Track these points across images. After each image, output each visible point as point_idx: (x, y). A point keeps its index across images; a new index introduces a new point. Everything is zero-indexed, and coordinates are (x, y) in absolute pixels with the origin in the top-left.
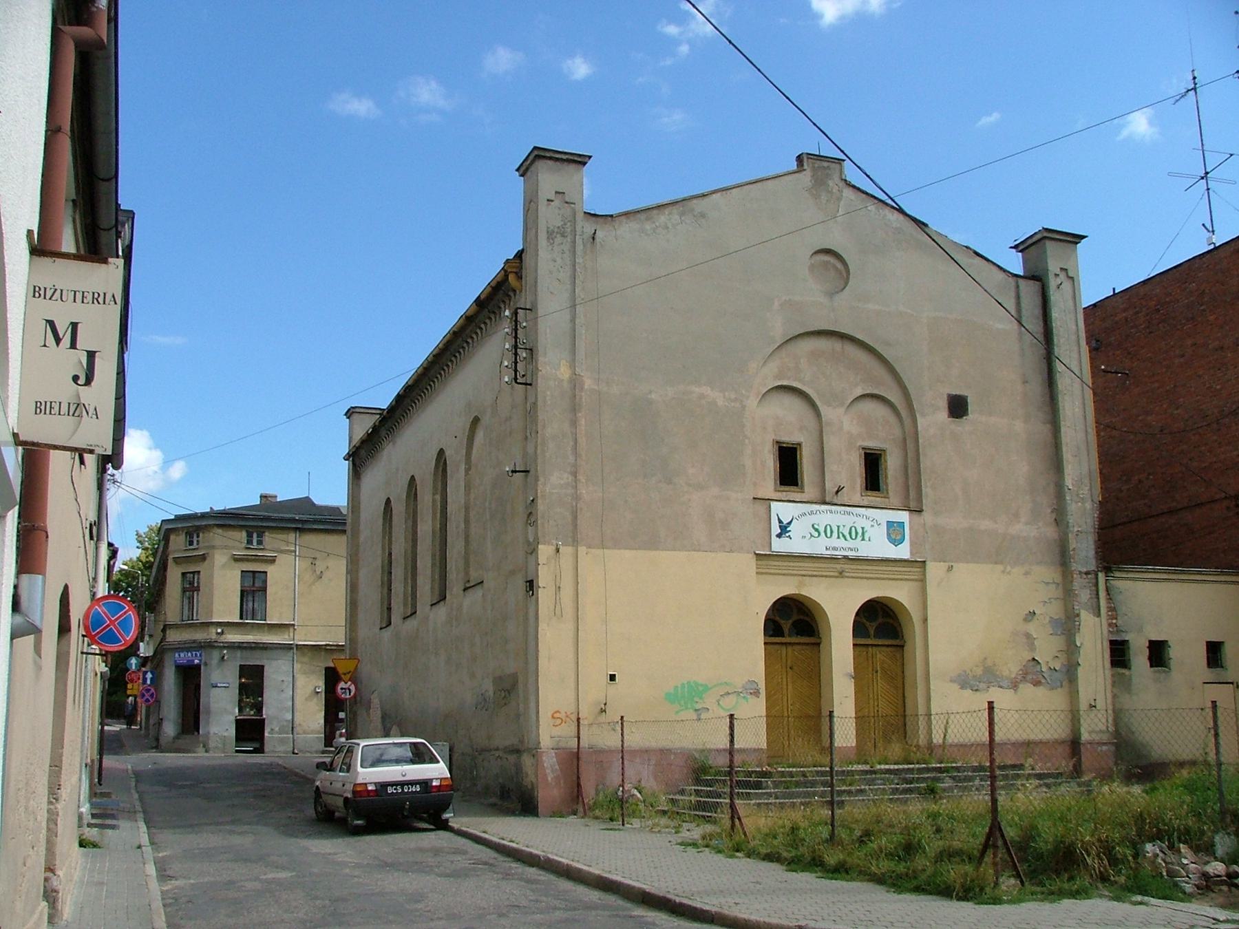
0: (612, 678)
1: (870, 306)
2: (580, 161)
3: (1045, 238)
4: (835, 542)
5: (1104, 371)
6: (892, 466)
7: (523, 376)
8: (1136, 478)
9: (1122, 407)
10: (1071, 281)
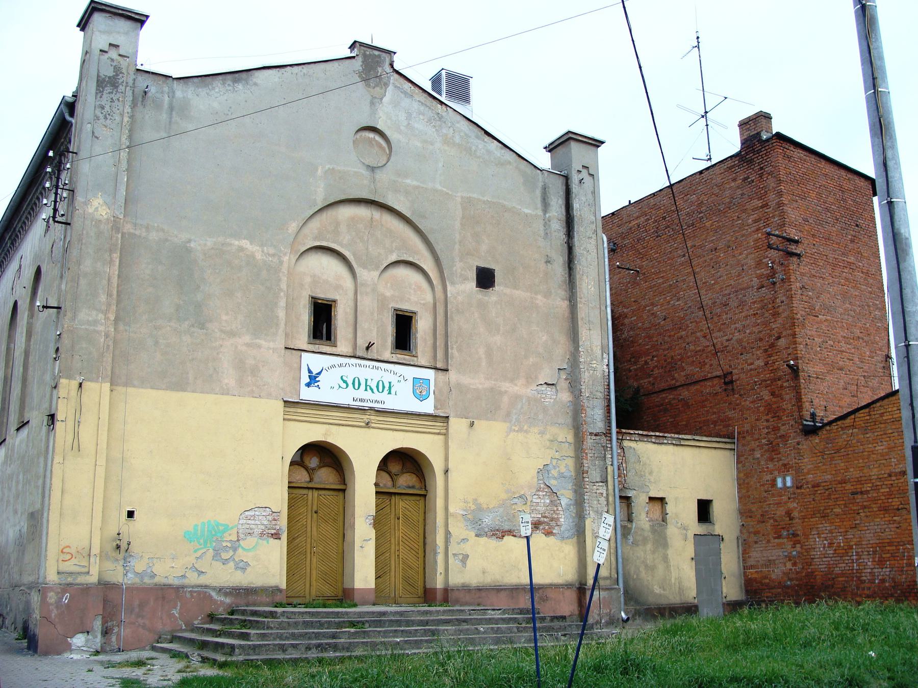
0: (131, 514)
1: (408, 181)
2: (139, 20)
3: (570, 138)
4: (361, 393)
5: (618, 267)
6: (422, 327)
7: (63, 215)
8: (643, 359)
9: (633, 300)
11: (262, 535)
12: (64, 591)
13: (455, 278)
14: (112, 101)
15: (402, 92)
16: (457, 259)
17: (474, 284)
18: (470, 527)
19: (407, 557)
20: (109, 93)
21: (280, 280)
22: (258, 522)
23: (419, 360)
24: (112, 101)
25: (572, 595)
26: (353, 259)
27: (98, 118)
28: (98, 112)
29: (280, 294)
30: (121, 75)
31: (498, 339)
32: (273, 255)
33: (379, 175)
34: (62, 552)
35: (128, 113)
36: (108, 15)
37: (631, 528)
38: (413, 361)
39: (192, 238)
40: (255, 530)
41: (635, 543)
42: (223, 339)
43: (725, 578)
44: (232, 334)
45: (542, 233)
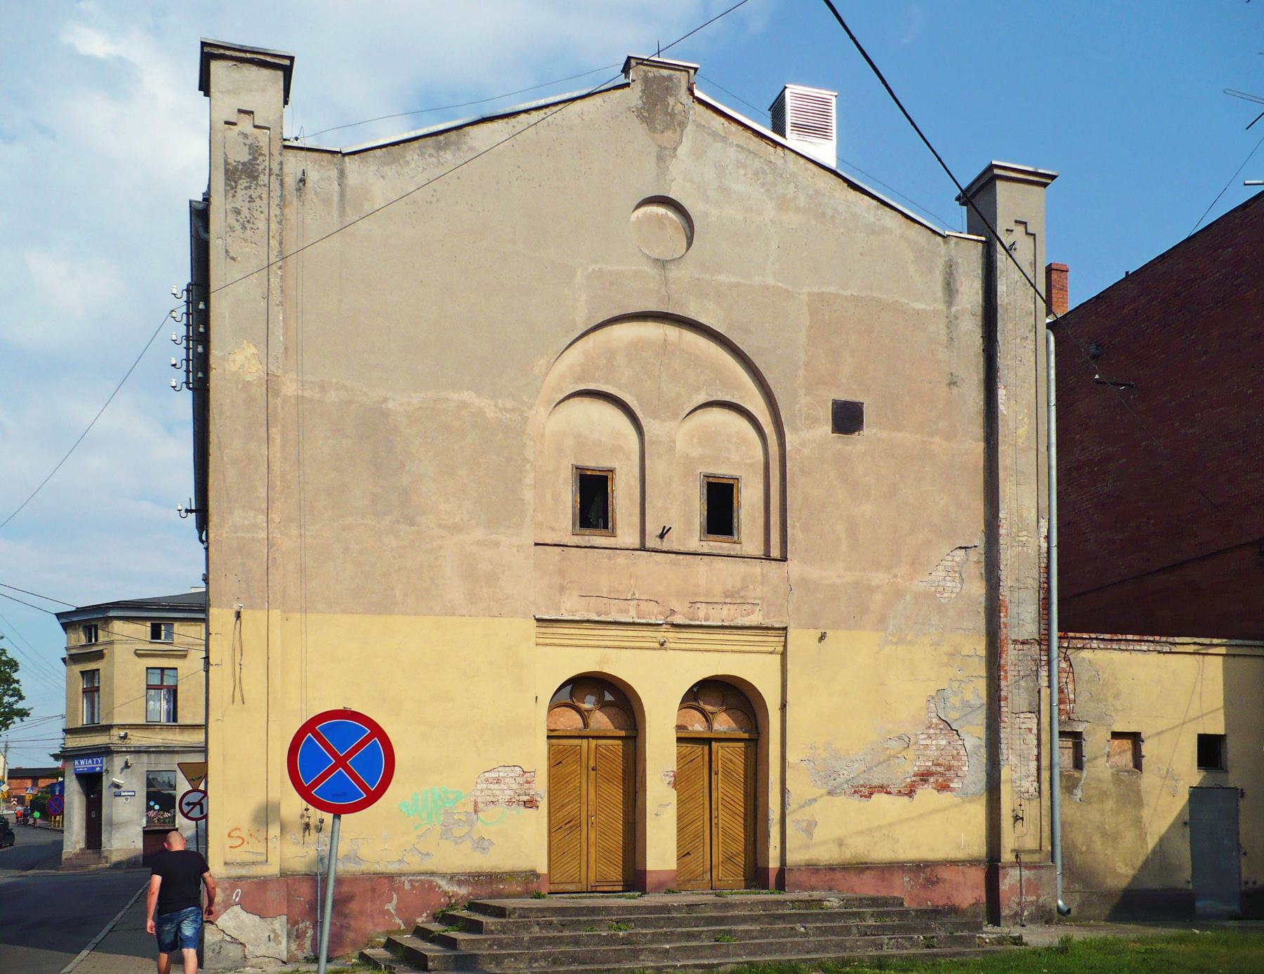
1: (722, 278)
5: (1098, 382)
6: (749, 501)
10: (1031, 239)
11: (510, 802)
12: (233, 888)
13: (798, 422)
14: (251, 200)
15: (709, 134)
16: (802, 392)
17: (829, 428)
18: (819, 783)
19: (728, 825)
20: (246, 188)
21: (524, 446)
22: (503, 786)
23: (744, 548)
24: (251, 200)
25: (977, 876)
26: (637, 405)
27: (232, 229)
28: (231, 219)
29: (524, 466)
30: (261, 158)
31: (867, 509)
32: (513, 410)
33: (674, 273)
34: (229, 836)
35: (276, 216)
36: (231, 63)
37: (1079, 779)
38: (734, 550)
39: (388, 395)
40: (500, 798)
41: (1085, 801)
42: (443, 537)
43: (1245, 854)
44: (456, 529)
45: (944, 339)
